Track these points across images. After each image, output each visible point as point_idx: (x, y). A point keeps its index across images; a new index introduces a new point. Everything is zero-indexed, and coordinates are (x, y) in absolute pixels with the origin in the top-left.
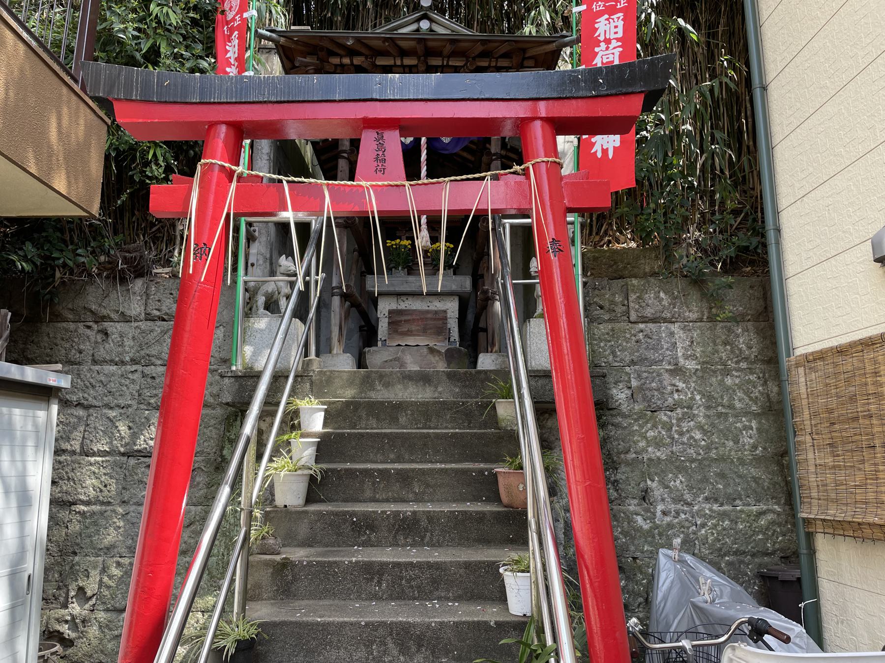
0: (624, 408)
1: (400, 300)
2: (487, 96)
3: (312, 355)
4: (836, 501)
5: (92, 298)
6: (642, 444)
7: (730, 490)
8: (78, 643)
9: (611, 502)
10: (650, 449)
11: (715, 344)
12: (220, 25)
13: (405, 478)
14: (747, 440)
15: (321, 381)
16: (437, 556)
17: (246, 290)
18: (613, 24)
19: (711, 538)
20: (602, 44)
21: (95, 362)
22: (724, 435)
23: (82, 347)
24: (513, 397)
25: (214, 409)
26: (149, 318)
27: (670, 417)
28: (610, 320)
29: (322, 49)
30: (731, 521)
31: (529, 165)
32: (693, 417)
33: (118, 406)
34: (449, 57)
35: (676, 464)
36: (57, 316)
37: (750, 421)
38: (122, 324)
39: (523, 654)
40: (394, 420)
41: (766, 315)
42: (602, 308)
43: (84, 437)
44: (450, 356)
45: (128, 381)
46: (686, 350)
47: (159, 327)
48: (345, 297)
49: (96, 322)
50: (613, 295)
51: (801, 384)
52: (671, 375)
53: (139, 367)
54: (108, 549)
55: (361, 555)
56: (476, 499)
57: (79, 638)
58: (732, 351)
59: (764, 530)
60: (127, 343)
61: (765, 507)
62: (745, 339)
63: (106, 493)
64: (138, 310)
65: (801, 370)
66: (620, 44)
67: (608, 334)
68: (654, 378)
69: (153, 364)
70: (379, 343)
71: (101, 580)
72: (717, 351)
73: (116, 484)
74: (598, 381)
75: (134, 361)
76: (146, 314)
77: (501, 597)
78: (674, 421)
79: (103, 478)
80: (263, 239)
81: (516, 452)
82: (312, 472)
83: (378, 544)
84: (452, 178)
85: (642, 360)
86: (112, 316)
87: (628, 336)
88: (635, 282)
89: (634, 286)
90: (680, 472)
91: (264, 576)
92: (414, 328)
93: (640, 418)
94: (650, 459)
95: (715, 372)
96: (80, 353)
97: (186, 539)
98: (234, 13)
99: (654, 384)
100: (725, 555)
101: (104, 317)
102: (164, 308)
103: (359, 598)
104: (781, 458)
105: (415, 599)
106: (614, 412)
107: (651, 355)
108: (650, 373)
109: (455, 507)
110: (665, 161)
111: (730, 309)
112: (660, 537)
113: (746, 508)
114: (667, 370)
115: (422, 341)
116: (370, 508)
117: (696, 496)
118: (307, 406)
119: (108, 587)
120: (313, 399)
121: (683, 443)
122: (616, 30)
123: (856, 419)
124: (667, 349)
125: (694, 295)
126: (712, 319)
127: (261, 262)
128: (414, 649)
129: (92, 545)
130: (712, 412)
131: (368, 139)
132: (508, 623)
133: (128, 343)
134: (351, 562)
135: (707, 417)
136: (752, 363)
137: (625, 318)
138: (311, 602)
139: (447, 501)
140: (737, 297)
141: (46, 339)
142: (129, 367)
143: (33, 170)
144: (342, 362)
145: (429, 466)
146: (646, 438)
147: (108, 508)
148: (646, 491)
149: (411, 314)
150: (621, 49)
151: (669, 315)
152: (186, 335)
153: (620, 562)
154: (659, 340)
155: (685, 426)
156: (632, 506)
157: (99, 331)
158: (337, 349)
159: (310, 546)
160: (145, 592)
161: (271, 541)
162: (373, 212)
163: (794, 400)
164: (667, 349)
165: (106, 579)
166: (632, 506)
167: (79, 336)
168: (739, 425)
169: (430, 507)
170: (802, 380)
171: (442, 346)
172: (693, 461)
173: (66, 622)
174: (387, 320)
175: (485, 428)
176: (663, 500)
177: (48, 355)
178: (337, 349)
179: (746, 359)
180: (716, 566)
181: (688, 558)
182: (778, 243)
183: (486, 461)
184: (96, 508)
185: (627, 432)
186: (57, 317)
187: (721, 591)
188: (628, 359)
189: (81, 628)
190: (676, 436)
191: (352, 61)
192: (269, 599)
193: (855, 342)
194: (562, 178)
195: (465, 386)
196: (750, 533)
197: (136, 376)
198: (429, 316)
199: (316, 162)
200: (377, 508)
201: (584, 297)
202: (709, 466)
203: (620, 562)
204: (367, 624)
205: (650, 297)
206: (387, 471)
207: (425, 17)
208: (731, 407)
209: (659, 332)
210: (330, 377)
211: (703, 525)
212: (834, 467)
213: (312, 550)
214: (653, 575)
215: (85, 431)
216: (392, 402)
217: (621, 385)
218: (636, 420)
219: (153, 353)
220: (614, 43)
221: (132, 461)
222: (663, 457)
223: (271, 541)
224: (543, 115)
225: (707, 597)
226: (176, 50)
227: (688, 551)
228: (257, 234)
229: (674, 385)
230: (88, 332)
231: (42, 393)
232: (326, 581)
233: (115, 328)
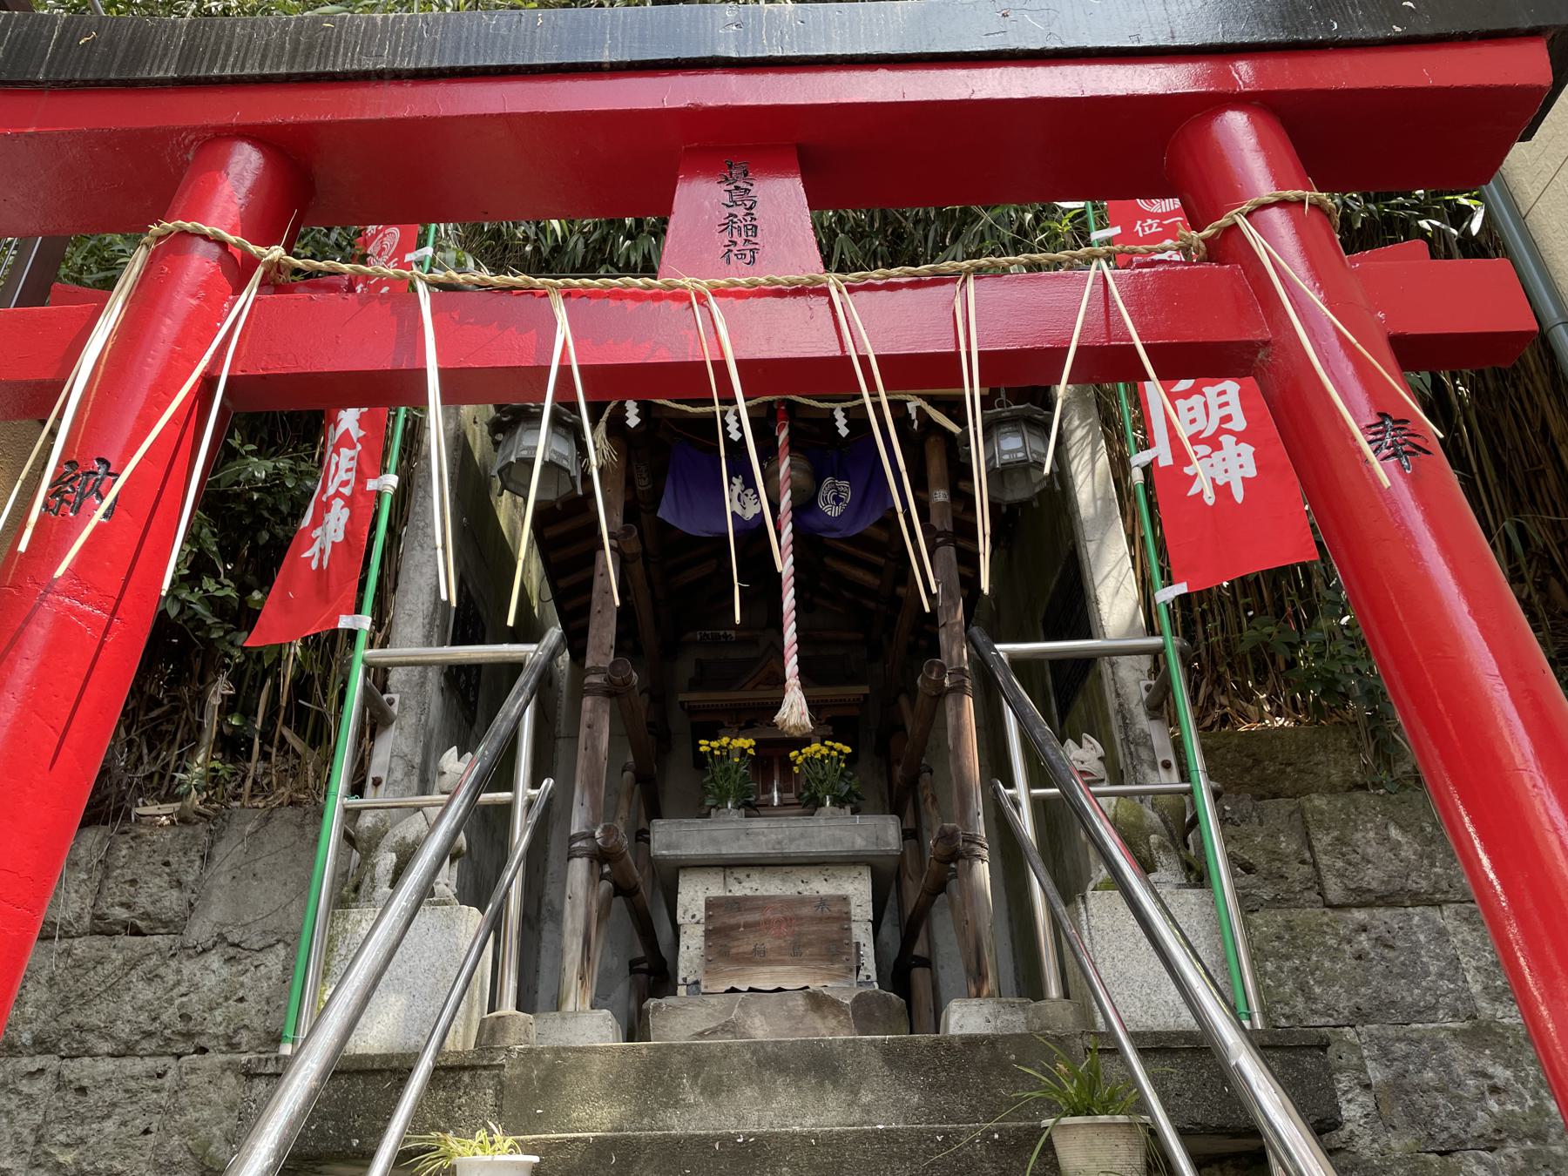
1: (730, 880)
3: (508, 1007)
15: (528, 1082)
17: (349, 839)
26: (102, 927)
28: (1276, 902)
44: (864, 1013)
45: (15, 1100)
47: (121, 951)
48: (600, 857)
50: (1273, 836)
52: (1469, 1046)
53: (51, 1062)
64: (76, 907)
67: (1279, 938)
70: (682, 991)
75: (42, 1045)
76: (96, 917)
80: (410, 720)
85: (1383, 1008)
87: (1332, 942)
88: (1320, 802)
89: (1322, 813)
92: (769, 942)
99: (1429, 1075)
102: (143, 901)
108: (1411, 1042)
114: (1455, 1034)
118: (481, 1157)
120: (498, 1137)
124: (1441, 975)
127: (398, 775)
137: (1314, 896)
142: (25, 1060)
144: (589, 1027)
149: (762, 908)
151: (1424, 883)
154: (1414, 950)
158: (576, 997)
162: (721, 366)
164: (1441, 975)
171: (843, 991)
174: (700, 930)
178: (576, 997)
188: (1345, 1005)
195: (934, 1087)
198: (806, 911)
199: (548, 595)
205: (1366, 838)
209: (1408, 932)
210: (553, 1067)
216: (732, 1138)
219: (94, 1020)
228: (395, 709)
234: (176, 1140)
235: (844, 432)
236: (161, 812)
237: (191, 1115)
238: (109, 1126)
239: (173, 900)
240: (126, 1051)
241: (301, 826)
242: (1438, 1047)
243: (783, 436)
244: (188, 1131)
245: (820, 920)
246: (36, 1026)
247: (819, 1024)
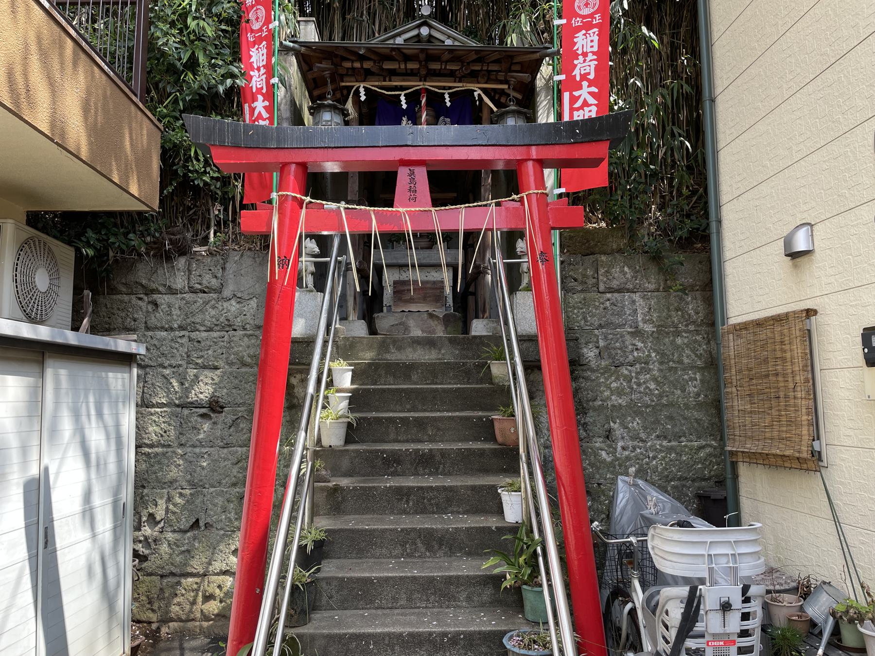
0: (593, 364)
2: (493, 143)
4: (751, 438)
5: (142, 273)
6: (607, 393)
7: (676, 430)
8: (152, 558)
9: (581, 440)
10: (613, 397)
11: (669, 310)
12: (244, 32)
13: (421, 423)
14: (692, 389)
15: (346, 346)
16: (449, 482)
18: (589, 39)
19: (660, 468)
20: (581, 57)
21: (148, 328)
22: (674, 385)
23: (135, 316)
24: (505, 359)
25: (252, 367)
26: (193, 290)
27: (630, 371)
28: (582, 291)
29: (337, 56)
30: (677, 454)
31: (524, 195)
32: (649, 371)
33: (171, 366)
34: (447, 62)
35: (634, 409)
36: (112, 289)
37: (695, 374)
38: (169, 296)
39: (518, 546)
40: (407, 378)
41: (709, 286)
42: (576, 280)
43: (143, 392)
44: (447, 320)
46: (645, 315)
49: (146, 294)
50: (585, 269)
51: (732, 347)
52: (632, 337)
54: (171, 483)
55: (392, 482)
56: (476, 439)
57: (153, 554)
58: (683, 316)
59: (702, 461)
60: (174, 313)
61: (704, 443)
62: (693, 306)
63: (166, 438)
65: (731, 336)
66: (595, 57)
68: (618, 339)
69: (198, 330)
70: (385, 309)
71: (167, 508)
72: (670, 316)
73: (175, 430)
74: (572, 344)
75: (181, 328)
76: (189, 287)
77: (500, 511)
78: (634, 375)
79: (163, 426)
81: (507, 402)
82: (349, 420)
83: (403, 474)
84: (467, 205)
85: (608, 324)
86: (161, 289)
87: (597, 304)
88: (603, 258)
90: (637, 416)
91: (321, 498)
93: (606, 372)
94: (613, 406)
95: (668, 333)
96: (135, 321)
97: (235, 474)
98: (261, 24)
100: (671, 480)
101: (154, 290)
102: (204, 282)
103: (392, 513)
104: (716, 406)
105: (434, 513)
106: (584, 368)
107: (616, 320)
109: (460, 445)
110: (631, 154)
111: (685, 280)
112: (619, 467)
113: (689, 444)
114: (629, 333)
115: (423, 308)
116: (397, 447)
117: (649, 434)
119: (174, 513)
121: (640, 392)
122: (592, 44)
123: (767, 376)
125: (653, 269)
126: (667, 289)
128: (436, 547)
129: (158, 480)
130: (664, 367)
131: (403, 174)
132: (505, 527)
133: (176, 312)
134: (386, 487)
135: (660, 370)
136: (698, 326)
138: (357, 516)
139: (454, 441)
140: (687, 274)
141: (104, 309)
143: (116, 180)
144: (359, 329)
145: (438, 414)
146: (610, 388)
147: (169, 450)
148: (610, 431)
150: (596, 63)
152: (274, 324)
153: (587, 487)
154: (623, 307)
155: (642, 378)
156: (598, 443)
157: (149, 302)
159: (351, 476)
160: (257, 506)
161: (324, 472)
162: (408, 231)
163: (725, 360)
165: (171, 507)
166: (598, 443)
167: (133, 307)
168: (686, 377)
169: (442, 446)
170: (732, 344)
171: (440, 312)
172: (647, 406)
173: (140, 542)
175: (481, 383)
176: (623, 438)
177: (106, 323)
179: (694, 322)
180: (663, 489)
181: (640, 482)
182: (719, 232)
183: (482, 410)
184: (159, 450)
185: (595, 384)
186: (113, 291)
187: (664, 506)
188: (596, 323)
189: (153, 546)
190: (635, 387)
191: (362, 65)
192: (325, 514)
193: (768, 318)
194: (547, 205)
195: (463, 349)
196: (691, 463)
197: (185, 340)
198: (429, 286)
200: (403, 447)
201: (561, 271)
202: (661, 410)
203: (587, 487)
204: (402, 530)
205: (616, 271)
206: (407, 418)
207: (425, 24)
208: (680, 362)
209: (623, 301)
211: (654, 458)
212: (751, 412)
213: (354, 479)
214: (613, 497)
215: (144, 387)
217: (591, 345)
218: (602, 374)
219: (198, 321)
220: (590, 57)
221: (186, 412)
222: (624, 404)
223: (324, 472)
224: (535, 157)
225: (653, 510)
226: (213, 61)
227: (641, 478)
229: (634, 345)
230: (140, 303)
231: (126, 359)
232: (366, 501)
233: (163, 300)
234: (232, 356)
235: (448, 104)
236: (202, 250)
237: (236, 349)
238: (210, 352)
239: (214, 283)
240: (210, 330)
241: (254, 258)
242: (622, 336)
243: (424, 101)
244: (236, 354)
245: (433, 289)
246: (179, 322)
247: (432, 323)
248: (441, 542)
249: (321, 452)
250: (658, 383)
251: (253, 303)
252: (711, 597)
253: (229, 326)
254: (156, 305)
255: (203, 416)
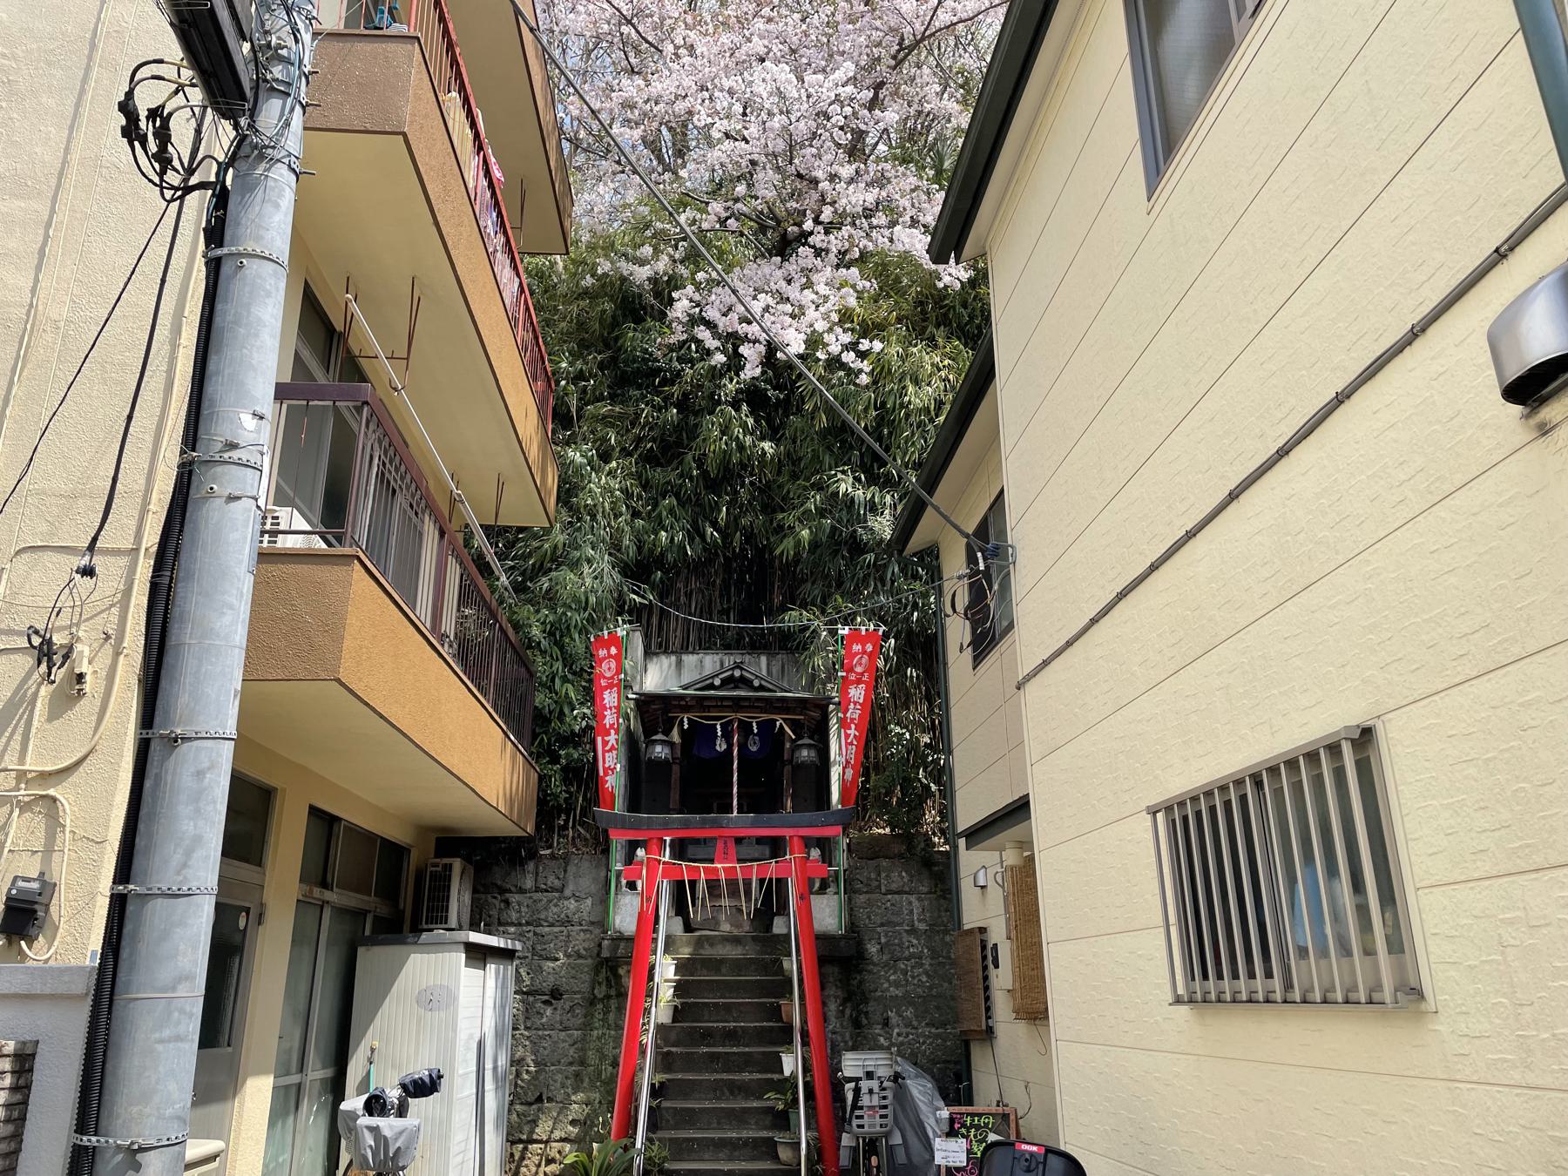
0: (875, 959)
13: (728, 1007)
35: (907, 1000)
40: (718, 972)
75: (528, 923)
77: (782, 1072)
85: (889, 923)
107: (894, 919)
221: (531, 999)
232: (690, 1062)
233: (514, 898)
240: (552, 925)
248: (740, 1089)
249: (660, 1028)
250: (928, 976)
251: (589, 902)
252: (865, 1085)
253: (568, 922)
254: (507, 902)
255: (545, 1002)
